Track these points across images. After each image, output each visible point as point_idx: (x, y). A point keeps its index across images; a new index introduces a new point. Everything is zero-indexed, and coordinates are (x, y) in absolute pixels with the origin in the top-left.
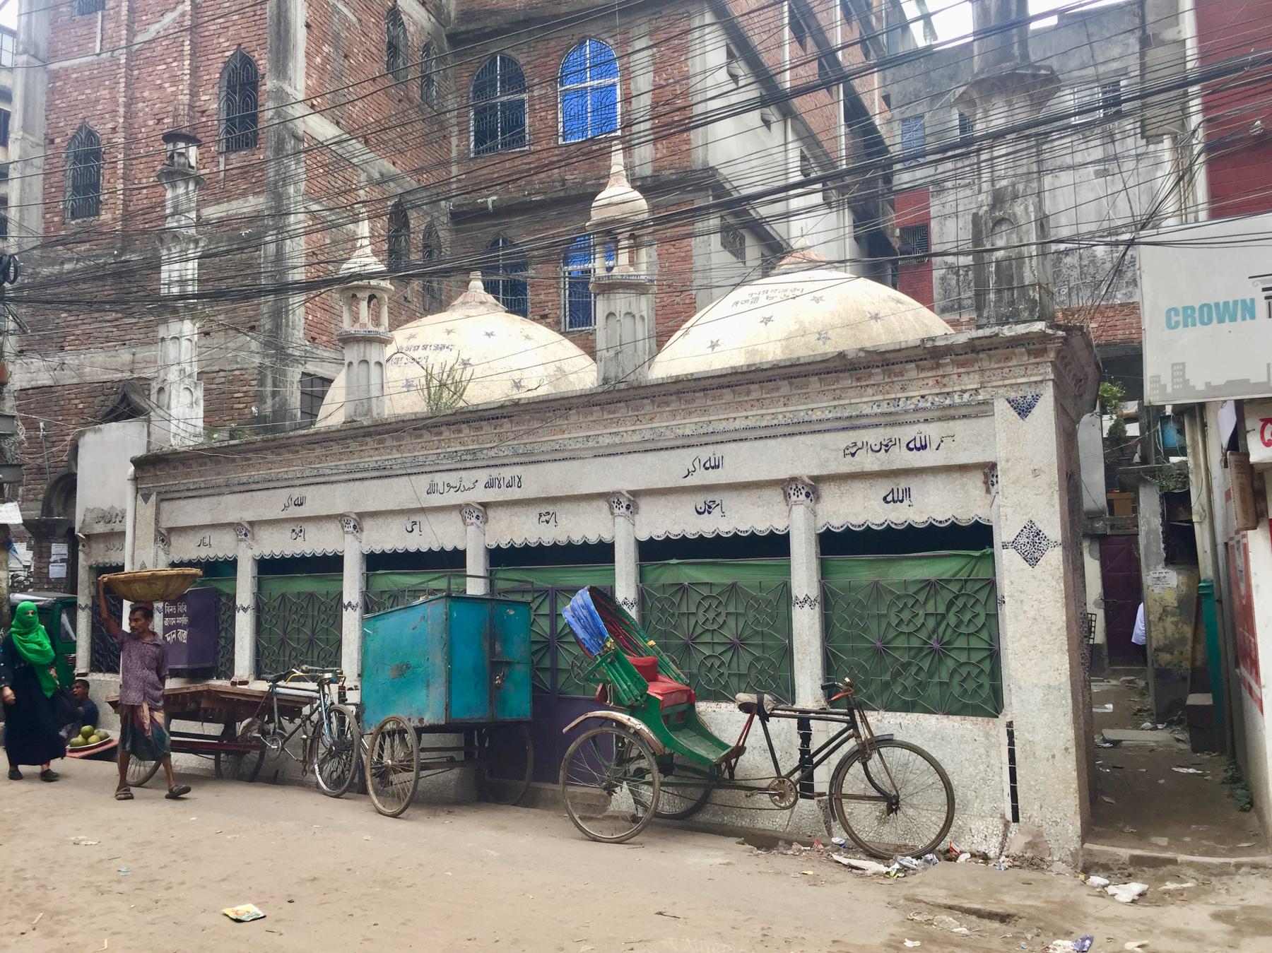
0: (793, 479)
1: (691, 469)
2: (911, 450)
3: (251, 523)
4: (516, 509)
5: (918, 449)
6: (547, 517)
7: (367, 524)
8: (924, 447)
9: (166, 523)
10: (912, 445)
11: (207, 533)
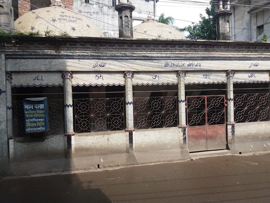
0: (128, 72)
1: (95, 66)
2: (100, 66)
3: (72, 71)
4: (196, 73)
5: (102, 67)
6: (206, 76)
7: (136, 75)
8: (104, 66)
9: (9, 69)
10: (101, 65)
11: (40, 75)
